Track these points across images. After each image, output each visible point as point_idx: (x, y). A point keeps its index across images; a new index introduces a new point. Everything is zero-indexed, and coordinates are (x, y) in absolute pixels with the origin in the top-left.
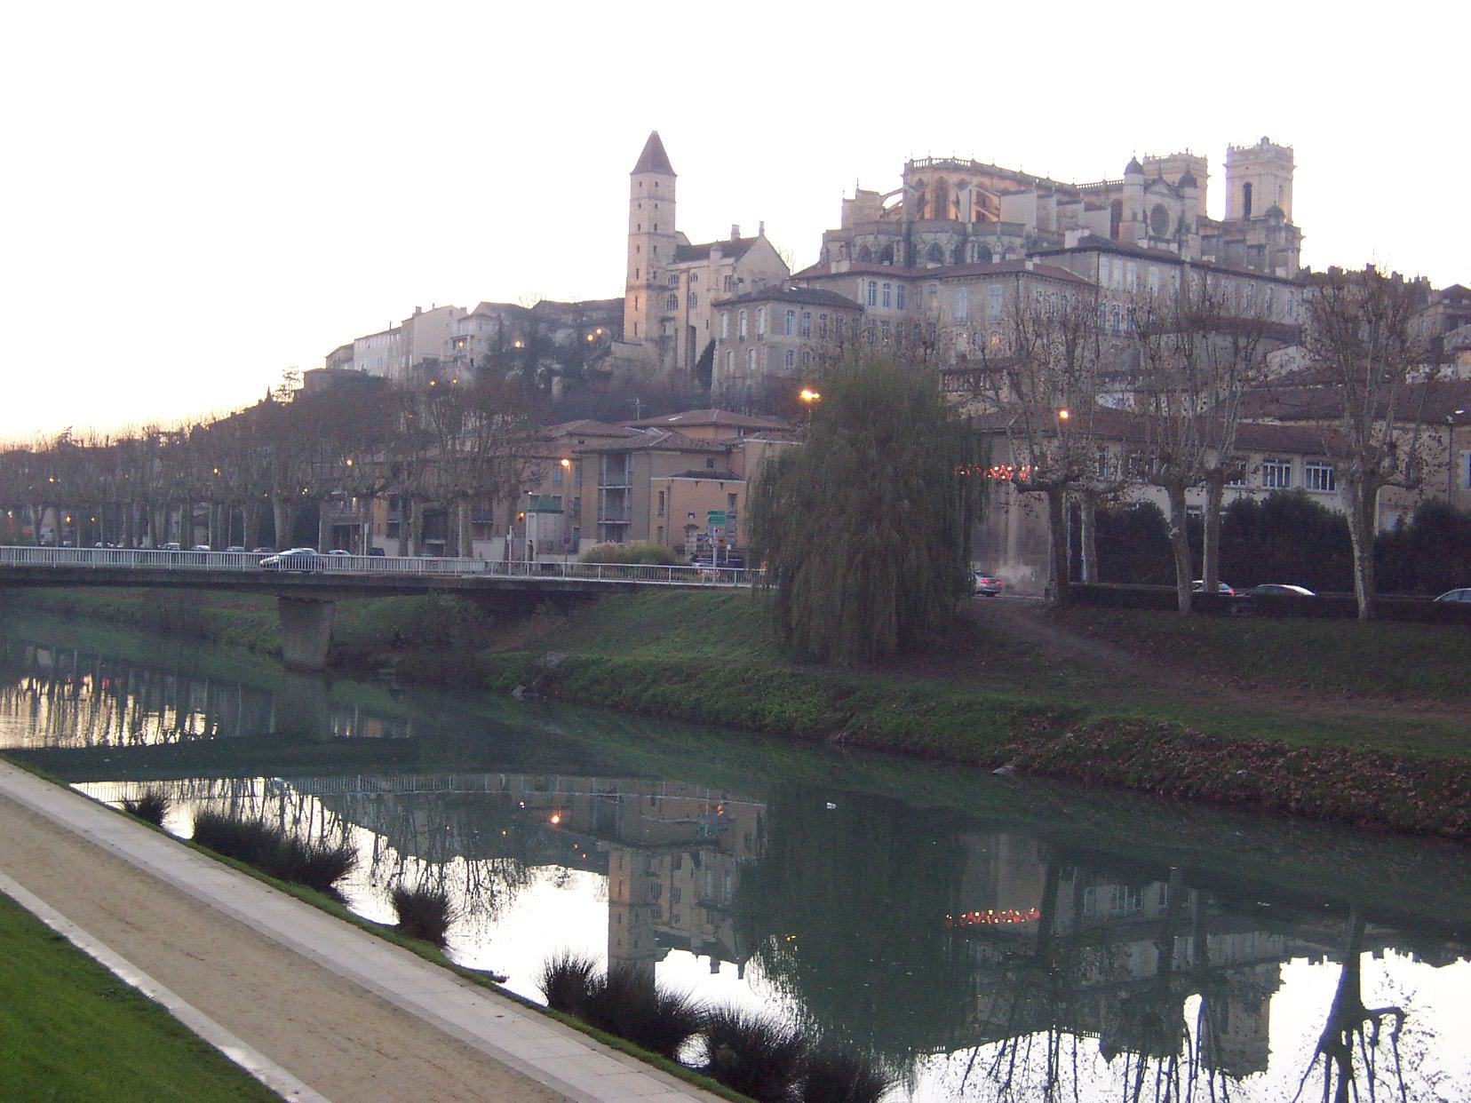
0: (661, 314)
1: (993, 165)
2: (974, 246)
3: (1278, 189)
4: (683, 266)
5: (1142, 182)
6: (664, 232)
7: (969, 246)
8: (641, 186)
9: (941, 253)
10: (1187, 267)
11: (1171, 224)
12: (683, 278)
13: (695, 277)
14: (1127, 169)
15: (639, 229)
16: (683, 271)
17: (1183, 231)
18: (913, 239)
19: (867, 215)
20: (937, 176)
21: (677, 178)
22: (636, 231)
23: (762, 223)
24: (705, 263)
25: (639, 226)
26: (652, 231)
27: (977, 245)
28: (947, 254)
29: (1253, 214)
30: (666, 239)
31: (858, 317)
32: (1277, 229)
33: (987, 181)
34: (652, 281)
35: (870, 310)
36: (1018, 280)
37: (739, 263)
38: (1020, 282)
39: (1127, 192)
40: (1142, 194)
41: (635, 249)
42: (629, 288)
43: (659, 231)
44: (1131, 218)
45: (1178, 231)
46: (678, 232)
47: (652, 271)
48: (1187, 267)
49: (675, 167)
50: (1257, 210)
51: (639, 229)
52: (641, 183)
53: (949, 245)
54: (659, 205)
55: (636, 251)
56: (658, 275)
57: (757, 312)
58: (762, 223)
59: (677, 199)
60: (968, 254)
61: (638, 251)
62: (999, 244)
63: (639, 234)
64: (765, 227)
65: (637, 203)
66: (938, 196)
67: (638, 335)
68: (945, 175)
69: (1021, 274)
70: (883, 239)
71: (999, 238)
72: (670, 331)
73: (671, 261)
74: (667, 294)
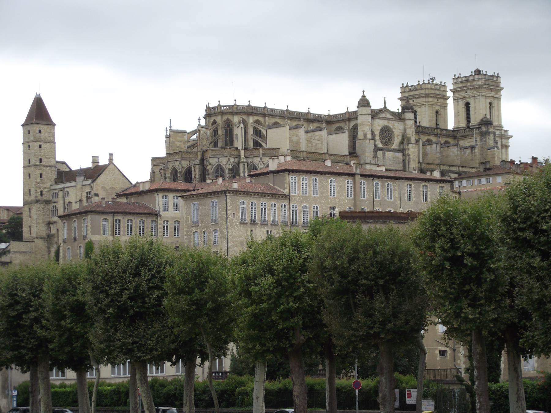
0: (48, 220)
1: (265, 107)
2: (244, 165)
3: (488, 105)
4: (60, 186)
5: (369, 112)
6: (47, 164)
7: (241, 166)
8: (29, 133)
9: (223, 171)
10: (357, 177)
11: (396, 138)
12: (61, 194)
13: (68, 193)
14: (359, 103)
15: (30, 163)
16: (60, 190)
17: (405, 142)
18: (205, 162)
19: (178, 147)
20: (225, 117)
21: (56, 127)
22: (28, 165)
23: (111, 155)
24: (73, 184)
25: (29, 160)
26: (38, 163)
27: (246, 164)
28: (227, 171)
29: (472, 123)
30: (48, 168)
31: (155, 219)
32: (487, 133)
33: (261, 119)
34: (39, 197)
35: (162, 213)
36: (226, 196)
37: (95, 183)
38: (228, 197)
39: (360, 120)
40: (370, 120)
41: (27, 176)
42: (25, 203)
43: (43, 163)
44: (363, 138)
45: (402, 143)
46: (58, 162)
47: (39, 190)
48: (357, 177)
49: (54, 117)
50: (475, 120)
51: (30, 163)
52: (29, 131)
53: (227, 166)
54: (42, 146)
55: (28, 177)
56: (44, 193)
57: (82, 221)
58: (111, 155)
59: (56, 140)
60: (241, 170)
61: (30, 178)
62: (261, 162)
63: (29, 166)
64: (114, 157)
65: (27, 145)
66: (226, 131)
67: (32, 235)
68: (230, 117)
69: (228, 192)
70: (185, 164)
71: (261, 159)
72: (53, 231)
73: (54, 183)
74: (52, 205)
